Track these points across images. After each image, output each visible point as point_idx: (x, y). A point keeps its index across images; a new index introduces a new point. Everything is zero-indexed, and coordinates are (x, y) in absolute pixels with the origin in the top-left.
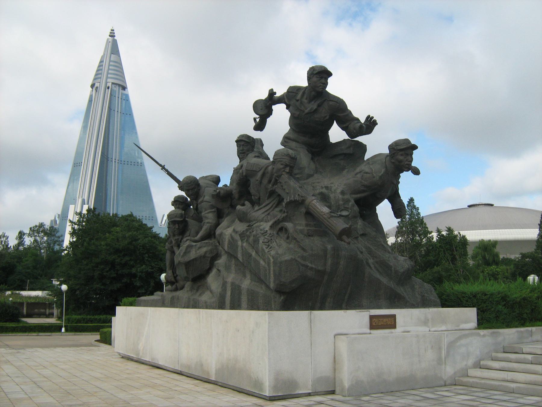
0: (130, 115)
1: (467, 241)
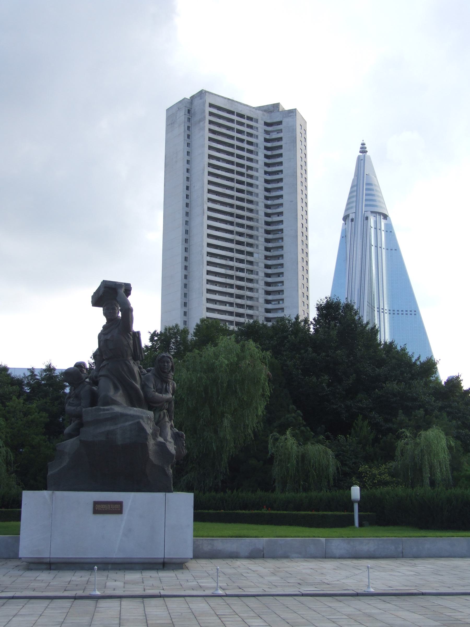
0: (396, 250)
1: (19, 380)
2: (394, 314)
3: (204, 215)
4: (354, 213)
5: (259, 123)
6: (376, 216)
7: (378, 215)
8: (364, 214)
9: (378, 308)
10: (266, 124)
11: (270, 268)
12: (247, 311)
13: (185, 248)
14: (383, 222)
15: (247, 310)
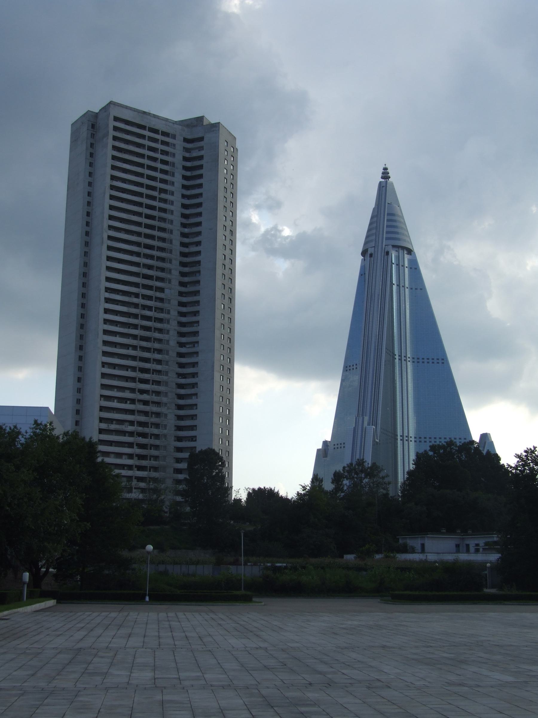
0: (421, 289)
2: (418, 362)
3: (102, 245)
4: (373, 248)
5: (176, 139)
6: (398, 251)
7: (401, 250)
8: (385, 248)
9: (400, 356)
10: (186, 140)
11: (186, 306)
12: (154, 355)
13: (83, 283)
14: (407, 257)
15: (154, 354)
